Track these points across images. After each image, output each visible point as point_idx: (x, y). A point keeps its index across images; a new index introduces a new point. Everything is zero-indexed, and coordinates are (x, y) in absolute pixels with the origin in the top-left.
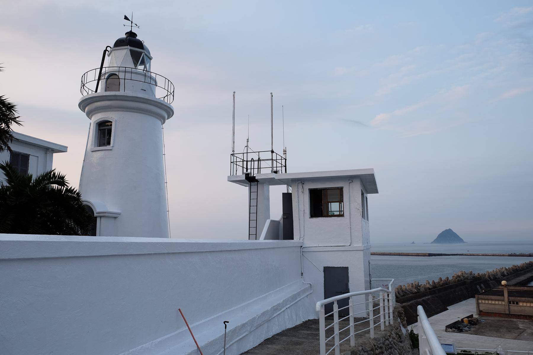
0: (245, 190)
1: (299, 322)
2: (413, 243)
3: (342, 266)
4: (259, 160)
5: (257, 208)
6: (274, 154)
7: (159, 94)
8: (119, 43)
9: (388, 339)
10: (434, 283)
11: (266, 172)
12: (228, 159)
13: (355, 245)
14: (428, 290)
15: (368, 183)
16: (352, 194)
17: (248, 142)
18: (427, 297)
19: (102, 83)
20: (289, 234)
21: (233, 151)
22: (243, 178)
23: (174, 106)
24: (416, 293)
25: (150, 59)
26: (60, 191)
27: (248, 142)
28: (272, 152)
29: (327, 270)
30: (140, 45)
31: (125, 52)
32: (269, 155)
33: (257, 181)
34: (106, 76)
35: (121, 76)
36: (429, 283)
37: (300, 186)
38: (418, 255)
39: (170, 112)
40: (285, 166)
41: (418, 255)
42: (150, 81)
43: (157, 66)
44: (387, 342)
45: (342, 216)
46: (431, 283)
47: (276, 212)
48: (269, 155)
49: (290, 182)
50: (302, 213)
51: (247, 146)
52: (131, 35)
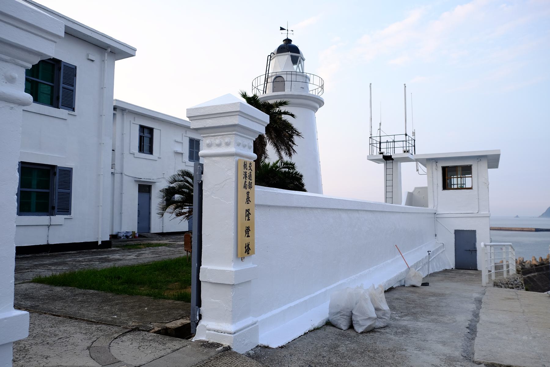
0: (382, 165)
1: (441, 270)
2: (517, 216)
3: (470, 229)
6: (407, 137)
7: (313, 89)
8: (281, 50)
9: (516, 280)
10: (542, 260)
11: (398, 152)
13: (482, 213)
14: (534, 267)
15: (493, 161)
17: (380, 125)
18: (533, 274)
19: (270, 85)
21: (371, 134)
22: (381, 157)
23: (323, 97)
25: (304, 60)
26: (289, 172)
27: (380, 125)
28: (406, 135)
29: (458, 233)
30: (295, 50)
31: (286, 57)
32: (403, 138)
33: (393, 159)
34: (273, 78)
35: (284, 76)
36: (535, 259)
37: (434, 164)
38: (522, 230)
39: (320, 103)
41: (522, 230)
42: (306, 79)
43: (308, 66)
44: (515, 282)
46: (538, 260)
48: (403, 138)
50: (435, 186)
51: (380, 129)
52: (288, 41)
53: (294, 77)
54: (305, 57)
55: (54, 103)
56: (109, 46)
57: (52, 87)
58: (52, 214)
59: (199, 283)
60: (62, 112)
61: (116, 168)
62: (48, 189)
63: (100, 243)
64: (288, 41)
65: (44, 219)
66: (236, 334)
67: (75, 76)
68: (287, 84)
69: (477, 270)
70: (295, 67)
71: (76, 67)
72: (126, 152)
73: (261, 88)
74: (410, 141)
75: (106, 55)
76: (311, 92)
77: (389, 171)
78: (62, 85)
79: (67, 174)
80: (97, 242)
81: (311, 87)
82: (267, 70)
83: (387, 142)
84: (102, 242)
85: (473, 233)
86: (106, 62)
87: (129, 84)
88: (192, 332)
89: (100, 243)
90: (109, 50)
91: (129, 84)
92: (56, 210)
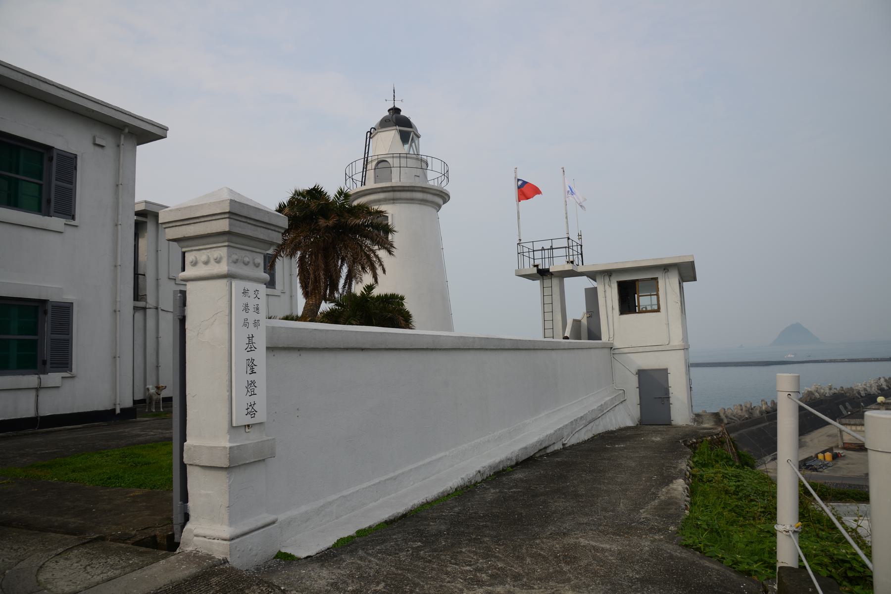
4: (552, 248)
5: (554, 306)
7: (433, 179)
8: (385, 123)
11: (559, 264)
12: (514, 250)
14: (765, 415)
15: (686, 272)
16: (668, 285)
19: (371, 174)
20: (594, 334)
22: (535, 270)
23: (448, 188)
24: (747, 419)
25: (418, 137)
28: (569, 239)
33: (552, 274)
34: (374, 163)
39: (444, 197)
40: (582, 254)
42: (423, 163)
43: (425, 147)
45: (658, 310)
46: (769, 404)
47: (577, 309)
48: (564, 243)
49: (593, 275)
53: (403, 161)
54: (420, 132)
55: (42, 208)
56: (126, 125)
57: (41, 185)
58: (45, 372)
59: (183, 467)
60: (56, 222)
61: (148, 300)
62: (36, 334)
63: (118, 411)
64: (395, 111)
65: (31, 380)
66: (233, 542)
67: (76, 169)
68: (395, 171)
69: (670, 424)
70: (407, 146)
71: (76, 156)
72: (163, 276)
73: (359, 177)
74: (575, 247)
75: (122, 137)
76: (431, 183)
77: (547, 291)
78: (54, 182)
79: (63, 313)
80: (114, 410)
81: (430, 175)
82: (366, 153)
83: (543, 249)
84: (121, 410)
85: (664, 372)
86: (122, 147)
87: (161, 178)
88: (176, 540)
89: (118, 411)
90: (127, 130)
91: (161, 178)
92: (48, 365)
